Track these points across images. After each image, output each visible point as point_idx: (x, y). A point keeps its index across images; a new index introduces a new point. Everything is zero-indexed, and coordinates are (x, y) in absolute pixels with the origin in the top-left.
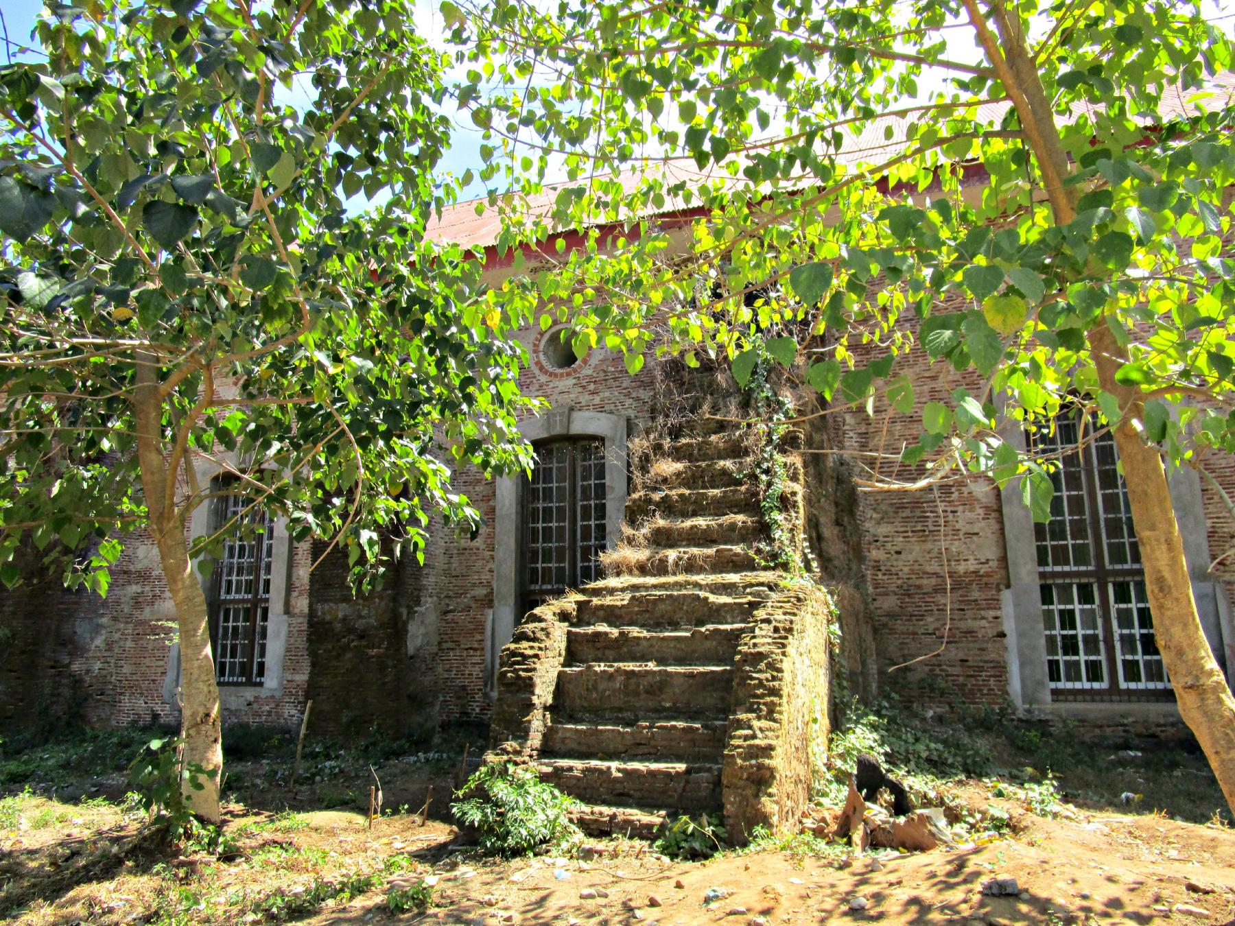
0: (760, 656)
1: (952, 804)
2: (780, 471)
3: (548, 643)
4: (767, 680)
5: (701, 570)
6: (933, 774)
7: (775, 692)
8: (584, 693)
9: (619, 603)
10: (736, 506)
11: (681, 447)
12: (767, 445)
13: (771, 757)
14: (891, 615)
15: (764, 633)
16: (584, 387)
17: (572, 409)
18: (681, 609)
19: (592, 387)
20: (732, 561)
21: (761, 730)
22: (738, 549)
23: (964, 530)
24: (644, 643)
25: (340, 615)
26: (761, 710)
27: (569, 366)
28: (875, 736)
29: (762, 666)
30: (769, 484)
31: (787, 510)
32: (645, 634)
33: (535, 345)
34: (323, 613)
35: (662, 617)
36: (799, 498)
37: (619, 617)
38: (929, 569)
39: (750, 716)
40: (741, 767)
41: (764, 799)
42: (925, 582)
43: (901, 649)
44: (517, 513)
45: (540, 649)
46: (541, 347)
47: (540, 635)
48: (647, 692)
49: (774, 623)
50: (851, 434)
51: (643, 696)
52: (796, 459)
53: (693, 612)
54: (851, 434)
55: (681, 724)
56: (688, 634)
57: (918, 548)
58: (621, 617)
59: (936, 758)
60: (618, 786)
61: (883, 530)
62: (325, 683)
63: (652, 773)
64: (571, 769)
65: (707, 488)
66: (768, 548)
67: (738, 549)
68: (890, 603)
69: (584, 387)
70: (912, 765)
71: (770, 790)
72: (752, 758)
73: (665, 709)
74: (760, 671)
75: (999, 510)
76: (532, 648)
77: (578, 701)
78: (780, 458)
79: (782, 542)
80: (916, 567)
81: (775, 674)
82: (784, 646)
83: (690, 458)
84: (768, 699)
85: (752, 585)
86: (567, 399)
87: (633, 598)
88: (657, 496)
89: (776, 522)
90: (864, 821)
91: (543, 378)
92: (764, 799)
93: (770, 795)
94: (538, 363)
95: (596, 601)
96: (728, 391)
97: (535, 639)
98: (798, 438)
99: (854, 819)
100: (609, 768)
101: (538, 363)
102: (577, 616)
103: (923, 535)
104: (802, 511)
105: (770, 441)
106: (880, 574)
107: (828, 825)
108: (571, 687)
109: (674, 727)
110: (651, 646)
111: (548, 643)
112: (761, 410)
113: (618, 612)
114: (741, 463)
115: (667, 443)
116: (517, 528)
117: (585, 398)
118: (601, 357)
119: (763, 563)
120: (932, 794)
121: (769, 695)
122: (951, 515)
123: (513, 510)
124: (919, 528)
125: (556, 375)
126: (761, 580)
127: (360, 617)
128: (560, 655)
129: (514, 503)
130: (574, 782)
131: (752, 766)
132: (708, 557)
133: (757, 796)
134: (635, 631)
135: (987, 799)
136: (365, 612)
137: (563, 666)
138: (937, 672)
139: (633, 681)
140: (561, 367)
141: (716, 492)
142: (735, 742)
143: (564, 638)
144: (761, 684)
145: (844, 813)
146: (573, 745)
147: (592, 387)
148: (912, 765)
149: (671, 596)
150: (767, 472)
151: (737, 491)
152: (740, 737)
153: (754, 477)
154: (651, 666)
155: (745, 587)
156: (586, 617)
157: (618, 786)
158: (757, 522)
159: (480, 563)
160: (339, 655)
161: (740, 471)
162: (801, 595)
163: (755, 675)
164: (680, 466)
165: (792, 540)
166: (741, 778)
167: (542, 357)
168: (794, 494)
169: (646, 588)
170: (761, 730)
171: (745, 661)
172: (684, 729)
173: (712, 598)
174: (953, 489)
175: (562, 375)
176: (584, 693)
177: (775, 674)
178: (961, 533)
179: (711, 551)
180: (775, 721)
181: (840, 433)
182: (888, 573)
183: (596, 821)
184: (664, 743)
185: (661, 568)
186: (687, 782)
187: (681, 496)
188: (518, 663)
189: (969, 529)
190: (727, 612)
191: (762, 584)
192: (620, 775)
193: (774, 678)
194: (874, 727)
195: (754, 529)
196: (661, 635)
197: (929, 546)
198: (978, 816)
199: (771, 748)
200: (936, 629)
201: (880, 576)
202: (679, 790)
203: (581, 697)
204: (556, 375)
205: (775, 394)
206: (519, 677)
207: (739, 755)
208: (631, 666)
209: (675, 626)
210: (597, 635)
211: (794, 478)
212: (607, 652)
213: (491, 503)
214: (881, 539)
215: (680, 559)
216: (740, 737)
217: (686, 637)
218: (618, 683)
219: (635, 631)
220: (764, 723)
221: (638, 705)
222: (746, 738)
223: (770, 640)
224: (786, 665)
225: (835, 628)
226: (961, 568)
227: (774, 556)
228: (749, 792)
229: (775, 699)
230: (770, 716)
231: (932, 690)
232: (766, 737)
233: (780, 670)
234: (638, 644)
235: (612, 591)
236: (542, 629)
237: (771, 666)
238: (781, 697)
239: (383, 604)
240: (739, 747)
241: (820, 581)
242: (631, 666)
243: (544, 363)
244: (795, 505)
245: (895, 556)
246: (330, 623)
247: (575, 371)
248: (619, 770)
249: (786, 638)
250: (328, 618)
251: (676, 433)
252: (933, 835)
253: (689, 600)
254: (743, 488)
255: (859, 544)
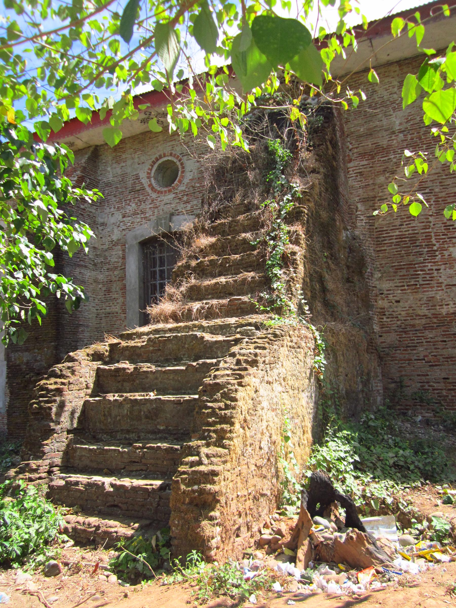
0: (217, 387)
1: (406, 510)
2: (285, 237)
3: (72, 379)
4: (220, 409)
5: (217, 316)
6: (392, 479)
7: (228, 420)
8: (102, 418)
9: (139, 345)
10: (250, 266)
11: (217, 226)
12: (277, 219)
13: (213, 482)
14: (390, 347)
15: (227, 365)
16: (180, 199)
17: (172, 215)
18: (183, 347)
19: (185, 198)
20: (241, 308)
21: (208, 456)
22: (245, 298)
23: (445, 283)
24: (151, 376)
25: (25, 360)
26: (210, 437)
27: (170, 186)
28: (347, 448)
29: (218, 395)
30: (275, 247)
31: (287, 267)
32: (154, 368)
33: (148, 173)
34: (15, 359)
35: (170, 354)
36: (298, 257)
37: (139, 355)
38: (420, 312)
39: (199, 442)
40: (184, 492)
41: (205, 523)
42: (417, 322)
43: (401, 371)
44: (140, 288)
45: (63, 384)
46: (152, 175)
47: (67, 373)
48: (147, 417)
49: (238, 357)
50: (362, 217)
51: (144, 421)
52: (298, 228)
53: (192, 349)
54: (362, 217)
55: (165, 445)
56: (183, 368)
57: (412, 298)
58: (140, 355)
59: (401, 463)
60: (110, 499)
61: (385, 285)
62: (18, 405)
63: (135, 489)
64: (77, 483)
65: (230, 255)
66: (267, 296)
67: (245, 298)
68: (391, 338)
69: (180, 199)
70: (378, 472)
71: (212, 514)
72: (195, 484)
73: (160, 431)
74: (215, 401)
75: (190, 65)
76: (56, 383)
77: (98, 424)
78: (285, 228)
79: (279, 290)
80: (411, 311)
81: (229, 402)
82: (241, 377)
83: (223, 233)
84: (219, 427)
85: (242, 326)
86: (169, 208)
87: (149, 340)
88: (194, 263)
89: (276, 275)
90: (310, 536)
91: (154, 195)
92: (205, 523)
93: (211, 519)
94: (150, 185)
95: (124, 344)
96: (254, 184)
97: (62, 376)
98: (302, 212)
99: (302, 534)
100: (103, 483)
101: (150, 185)
102: (110, 356)
103: (415, 288)
104: (301, 268)
105: (279, 217)
106: (384, 317)
107: (283, 536)
108: (92, 413)
109: (159, 447)
110: (156, 378)
111: (72, 379)
112: (276, 194)
113: (138, 351)
114: (257, 234)
115: (207, 224)
116: (140, 297)
117: (181, 207)
118: (191, 177)
119: (262, 308)
120: (389, 500)
121: (220, 423)
122: (435, 272)
123: (137, 286)
124: (412, 283)
125: (162, 192)
126: (250, 321)
127: (36, 361)
128: (87, 388)
129: (137, 281)
130: (79, 494)
131: (194, 491)
132: (223, 305)
133: (198, 521)
134: (146, 367)
135: (436, 505)
136: (39, 358)
137: (91, 396)
138: (427, 387)
139: (136, 408)
140: (167, 186)
141: (237, 256)
142: (182, 468)
143: (93, 374)
144: (213, 413)
145: (297, 525)
146: (87, 462)
147: (185, 198)
148: (378, 472)
149: (176, 337)
150: (274, 239)
151: (251, 254)
152: (186, 464)
153: (265, 243)
154: (152, 395)
155: (236, 328)
156: (116, 357)
157: (110, 499)
158: (263, 277)
159: (118, 322)
160: (26, 386)
161: (255, 240)
162: (278, 332)
163: (209, 404)
164: (213, 240)
165: (289, 289)
166: (183, 503)
167: (152, 180)
168: (294, 253)
169: (165, 331)
170: (208, 456)
171: (205, 391)
172: (166, 450)
173: (208, 337)
174: (437, 253)
175: (165, 192)
176: (102, 418)
177: (229, 402)
178: (443, 285)
179: (225, 301)
180: (224, 447)
181: (354, 217)
182: (391, 316)
183: (84, 531)
184: (152, 461)
185: (188, 316)
186: (160, 498)
187: (211, 261)
188: (42, 396)
189: (449, 281)
190: (217, 348)
191: (250, 324)
192: (112, 489)
193: (227, 407)
194: (347, 440)
195: (260, 282)
196: (163, 369)
197: (420, 296)
198: (425, 523)
199: (214, 473)
200: (425, 356)
201: (385, 320)
202: (155, 505)
203: (100, 422)
204: (162, 192)
205: (289, 182)
206: (41, 408)
207: (183, 480)
208: (138, 396)
209: (178, 360)
210: (118, 370)
211: (297, 242)
212: (125, 384)
213: (124, 282)
214: (385, 292)
215: (203, 308)
216: (186, 464)
217: (183, 370)
218: (125, 410)
219: (146, 367)
220: (212, 450)
221: (140, 427)
222: (192, 464)
223: (229, 372)
224: (241, 394)
225: (321, 359)
226: (444, 311)
227: (272, 302)
228: (190, 516)
229: (226, 427)
230: (219, 443)
231: (422, 401)
232: (211, 463)
233: (234, 400)
234: (147, 377)
235: (140, 335)
236: (69, 368)
237: (226, 396)
238: (232, 424)
239: (49, 351)
240: (184, 473)
241: (312, 321)
242: (138, 396)
243: (154, 185)
244: (294, 262)
245: (396, 304)
246: (19, 365)
247: (174, 188)
248: (112, 485)
249: (246, 369)
250: (18, 362)
251: (214, 216)
252: (369, 552)
253: (189, 340)
254: (255, 252)
255: (367, 296)
